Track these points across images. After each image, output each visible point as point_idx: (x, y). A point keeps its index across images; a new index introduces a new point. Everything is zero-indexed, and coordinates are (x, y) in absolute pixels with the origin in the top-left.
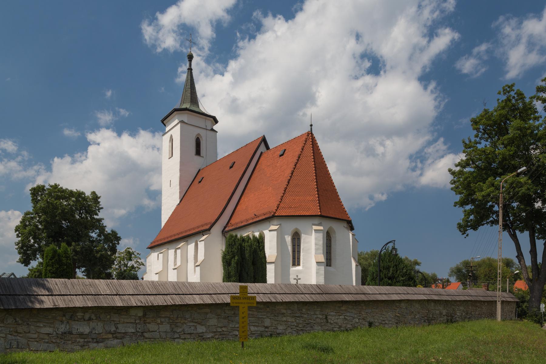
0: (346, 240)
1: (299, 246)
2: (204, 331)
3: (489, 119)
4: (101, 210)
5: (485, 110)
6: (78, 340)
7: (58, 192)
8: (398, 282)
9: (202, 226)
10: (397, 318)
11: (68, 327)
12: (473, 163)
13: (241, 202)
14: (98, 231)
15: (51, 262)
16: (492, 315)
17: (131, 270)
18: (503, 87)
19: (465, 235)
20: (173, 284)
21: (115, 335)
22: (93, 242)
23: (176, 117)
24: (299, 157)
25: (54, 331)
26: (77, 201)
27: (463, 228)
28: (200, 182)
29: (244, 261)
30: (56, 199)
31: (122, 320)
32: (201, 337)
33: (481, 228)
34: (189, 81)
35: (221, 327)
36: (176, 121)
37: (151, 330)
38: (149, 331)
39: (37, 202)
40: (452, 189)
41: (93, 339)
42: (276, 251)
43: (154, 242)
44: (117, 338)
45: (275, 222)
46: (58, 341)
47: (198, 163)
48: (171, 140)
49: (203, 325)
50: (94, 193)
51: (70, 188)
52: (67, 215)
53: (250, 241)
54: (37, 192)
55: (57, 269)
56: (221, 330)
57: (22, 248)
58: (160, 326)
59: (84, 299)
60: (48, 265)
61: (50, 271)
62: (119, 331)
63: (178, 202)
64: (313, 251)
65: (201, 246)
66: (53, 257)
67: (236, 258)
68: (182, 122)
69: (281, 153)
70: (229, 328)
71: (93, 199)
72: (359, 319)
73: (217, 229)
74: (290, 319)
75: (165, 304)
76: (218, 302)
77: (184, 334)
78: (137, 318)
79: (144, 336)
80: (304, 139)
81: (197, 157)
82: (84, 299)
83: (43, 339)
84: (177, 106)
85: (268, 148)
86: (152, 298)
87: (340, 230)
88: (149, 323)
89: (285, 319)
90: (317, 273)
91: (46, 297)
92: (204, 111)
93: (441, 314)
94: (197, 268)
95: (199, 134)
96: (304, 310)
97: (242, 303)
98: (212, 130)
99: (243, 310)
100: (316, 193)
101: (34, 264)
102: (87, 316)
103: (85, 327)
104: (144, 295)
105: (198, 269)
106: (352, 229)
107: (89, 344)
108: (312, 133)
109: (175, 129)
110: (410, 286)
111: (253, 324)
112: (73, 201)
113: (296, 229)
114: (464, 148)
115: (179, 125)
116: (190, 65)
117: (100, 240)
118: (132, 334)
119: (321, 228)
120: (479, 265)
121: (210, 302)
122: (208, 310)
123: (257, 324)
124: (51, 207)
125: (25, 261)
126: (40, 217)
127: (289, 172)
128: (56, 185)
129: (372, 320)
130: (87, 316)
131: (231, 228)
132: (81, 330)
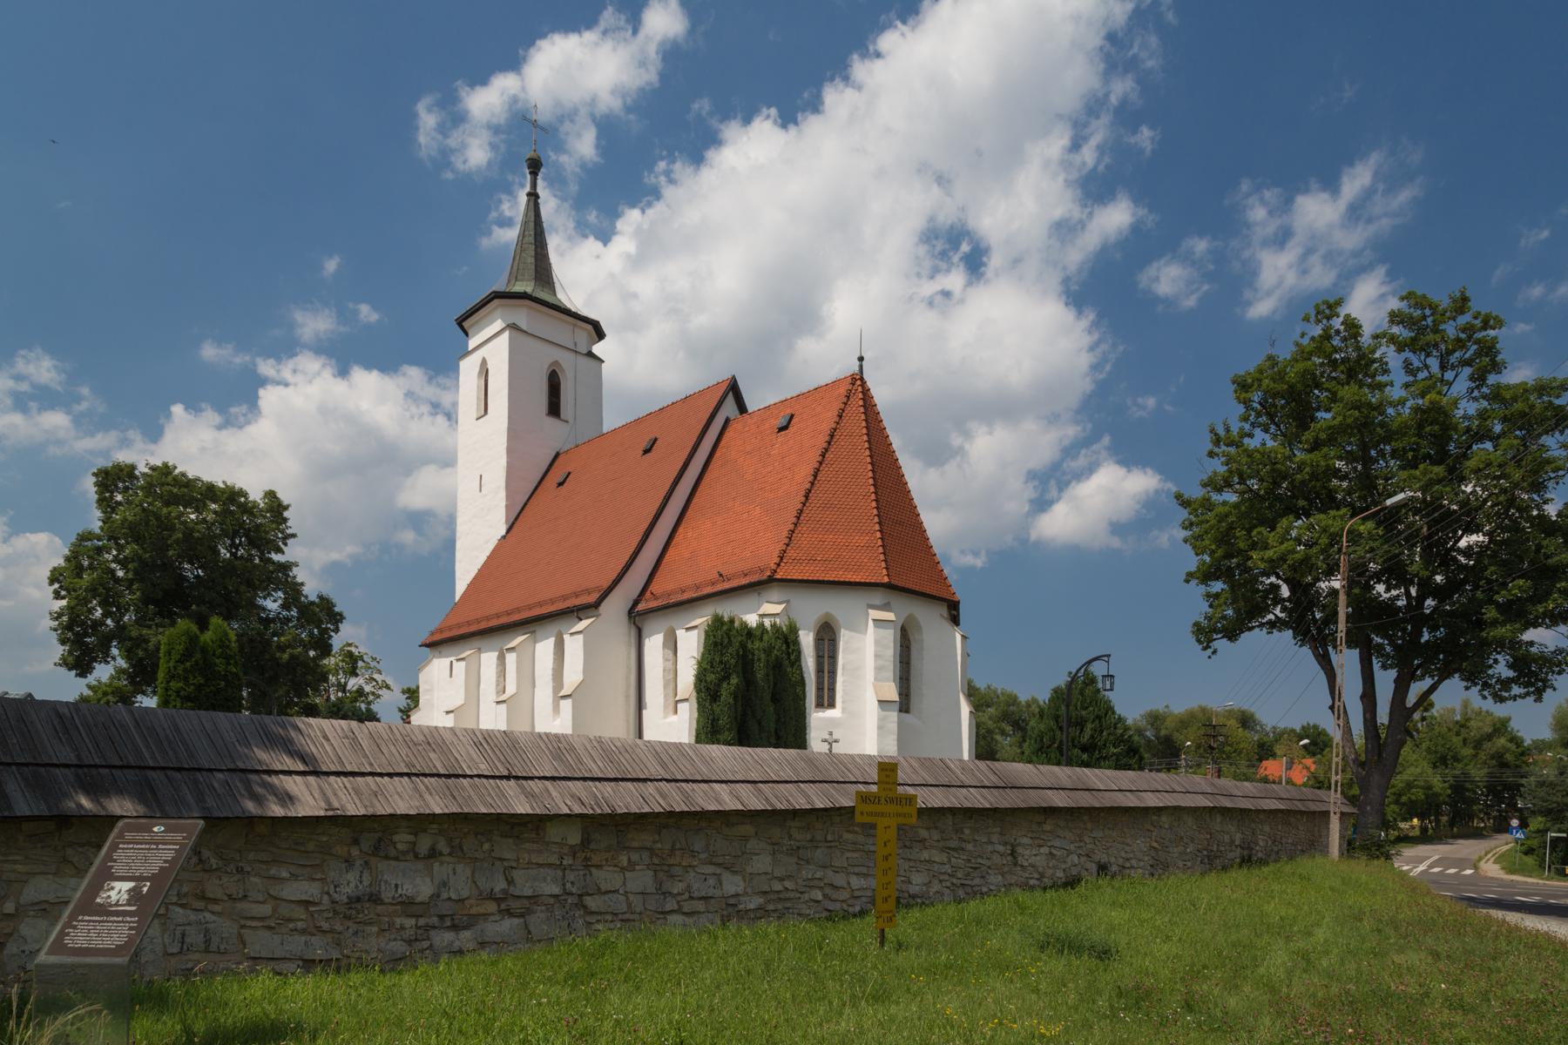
0: (947, 650)
1: (833, 657)
2: (740, 890)
3: (1281, 376)
4: (289, 542)
5: (1270, 358)
6: (398, 921)
7: (173, 488)
8: (1105, 758)
9: (577, 595)
10: (1153, 853)
11: (366, 880)
12: (1242, 481)
13: (677, 539)
14: (280, 594)
15: (181, 668)
16: (1315, 845)
17: (356, 700)
18: (1317, 306)
19: (1209, 651)
20: (555, 744)
21: (506, 904)
22: (267, 621)
23: (499, 312)
24: (832, 436)
25: (323, 893)
26: (224, 514)
27: (1205, 634)
28: (560, 484)
29: (757, 692)
30: (167, 504)
31: (526, 856)
32: (731, 911)
33: (1246, 636)
34: (532, 225)
35: (781, 879)
36: (498, 325)
37: (603, 889)
38: (600, 892)
39: (113, 510)
40: (1185, 541)
41: (441, 917)
43: (440, 630)
44: (509, 913)
45: (775, 594)
46: (338, 927)
47: (554, 435)
48: (484, 372)
49: (735, 872)
50: (271, 495)
51: (206, 478)
52: (197, 546)
53: (765, 637)
54: (112, 479)
55: (199, 687)
56: (780, 888)
57: (69, 627)
58: (628, 874)
59: (416, 789)
60: (173, 677)
61: (178, 692)
62: (517, 893)
64: (870, 674)
65: (574, 646)
66: (187, 655)
67: (734, 680)
68: (512, 327)
69: (782, 422)
70: (800, 881)
71: (270, 509)
72: (1079, 856)
73: (616, 606)
74: (938, 857)
75: (647, 810)
76: (779, 806)
77: (691, 898)
78: (566, 850)
79: (585, 907)
80: (843, 391)
81: (552, 421)
82: (416, 789)
83: (290, 920)
84: (500, 286)
85: (742, 409)
86: (608, 788)
87: (931, 620)
88: (599, 867)
89: (925, 855)
90: (880, 728)
91: (298, 778)
92: (569, 305)
93: (1232, 842)
94: (563, 702)
95: (556, 363)
96: (967, 831)
97: (882, 815)
98: (590, 354)
99: (886, 831)
100: (877, 527)
101: (103, 672)
102: (424, 844)
103: (418, 880)
104: (585, 779)
105: (566, 705)
106: (955, 620)
107: (432, 933)
108: (862, 379)
109: (492, 347)
110: (1128, 767)
111: (856, 870)
112: (215, 512)
113: (827, 614)
114: (1210, 446)
115: (506, 334)
116: (534, 185)
117: (288, 620)
118: (552, 901)
119: (890, 616)
120: (1185, 722)
121: (760, 807)
122: (747, 829)
123: (864, 870)
124: (153, 522)
125: (80, 663)
126: (120, 548)
127: (804, 472)
128: (166, 465)
129: (1104, 859)
130: (424, 844)
131: (653, 604)
132: (407, 889)
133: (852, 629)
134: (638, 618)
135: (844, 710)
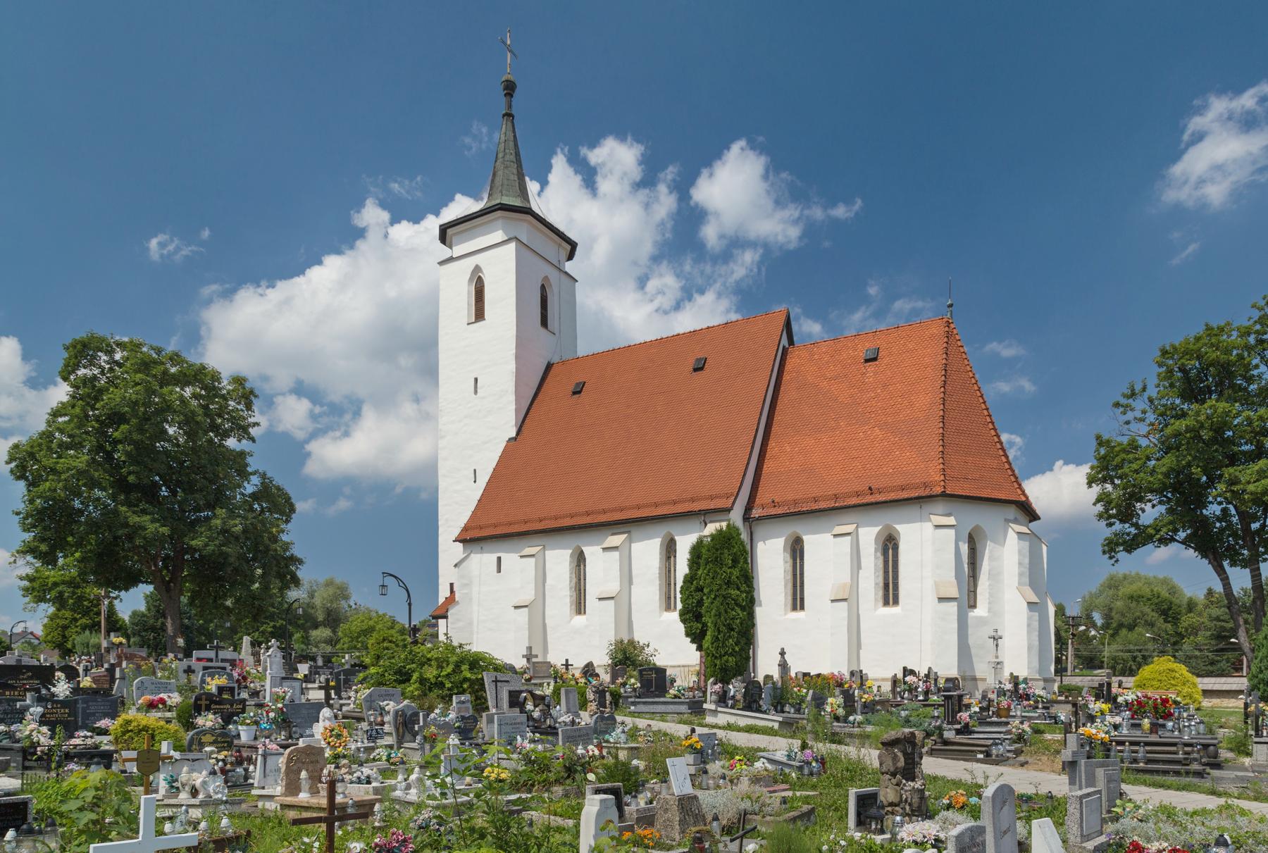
23: (500, 222)
36: (499, 236)
63: (514, 435)
81: (543, 330)
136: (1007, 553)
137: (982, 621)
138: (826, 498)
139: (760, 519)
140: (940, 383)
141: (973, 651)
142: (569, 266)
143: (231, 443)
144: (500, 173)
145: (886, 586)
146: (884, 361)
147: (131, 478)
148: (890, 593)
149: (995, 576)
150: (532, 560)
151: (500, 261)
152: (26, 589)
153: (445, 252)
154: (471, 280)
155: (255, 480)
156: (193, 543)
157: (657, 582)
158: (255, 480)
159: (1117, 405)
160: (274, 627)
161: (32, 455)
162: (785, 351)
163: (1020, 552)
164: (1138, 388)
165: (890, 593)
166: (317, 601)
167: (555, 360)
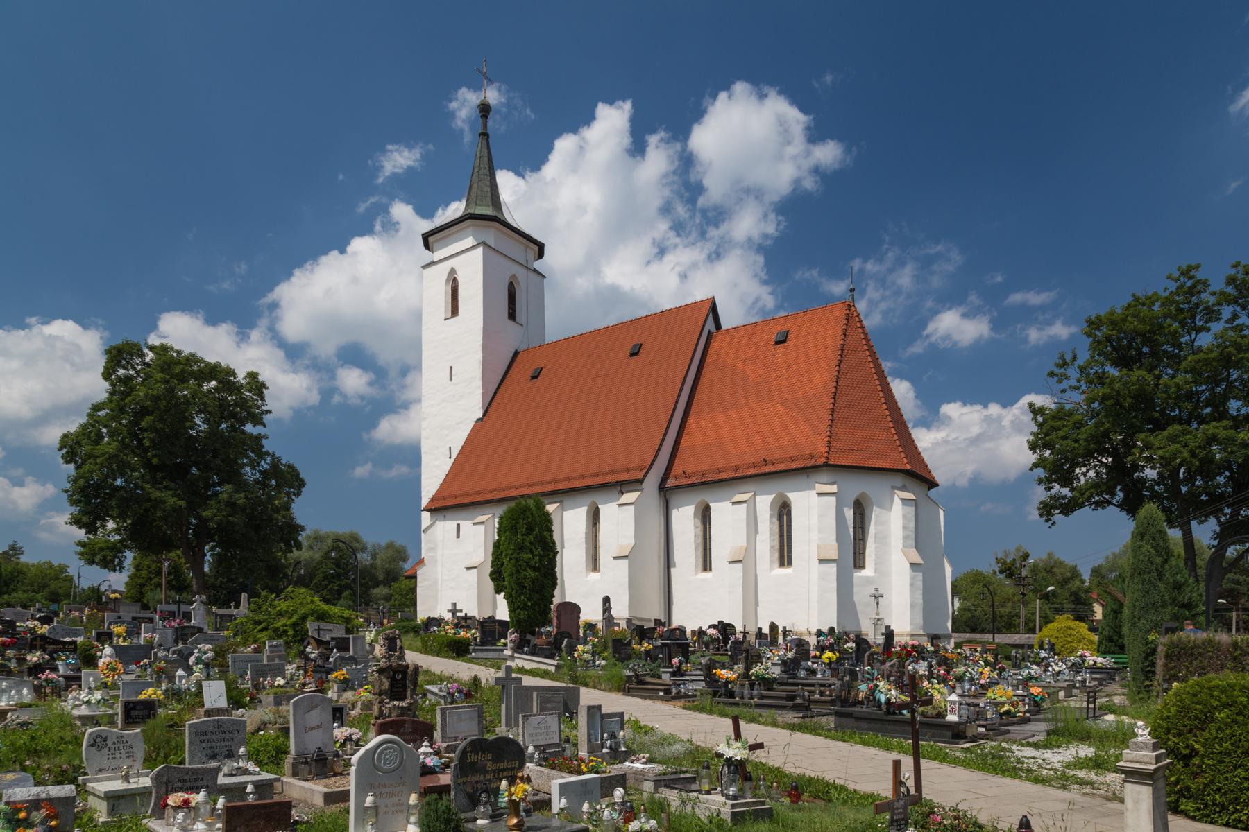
13: (688, 429)
23: (470, 230)
36: (469, 241)
42: (834, 537)
47: (513, 338)
63: (480, 416)
81: (511, 323)
113: (863, 494)
133: (880, 506)
134: (667, 493)
135: (876, 571)
136: (893, 519)
137: (868, 580)
138: (728, 469)
139: (672, 488)
140: (836, 362)
141: (859, 609)
142: (537, 265)
143: (249, 428)
144: (475, 186)
145: (782, 546)
146: (791, 343)
147: (155, 461)
148: (785, 557)
149: (883, 539)
150: (482, 527)
151: (468, 261)
152: (81, 554)
153: (428, 256)
154: (447, 281)
155: (269, 459)
156: (204, 514)
157: (584, 546)
158: (269, 459)
159: (1051, 374)
160: (340, 585)
161: (78, 443)
162: (710, 334)
163: (904, 517)
164: (1068, 358)
165: (785, 557)
166: (378, 562)
167: (521, 349)
